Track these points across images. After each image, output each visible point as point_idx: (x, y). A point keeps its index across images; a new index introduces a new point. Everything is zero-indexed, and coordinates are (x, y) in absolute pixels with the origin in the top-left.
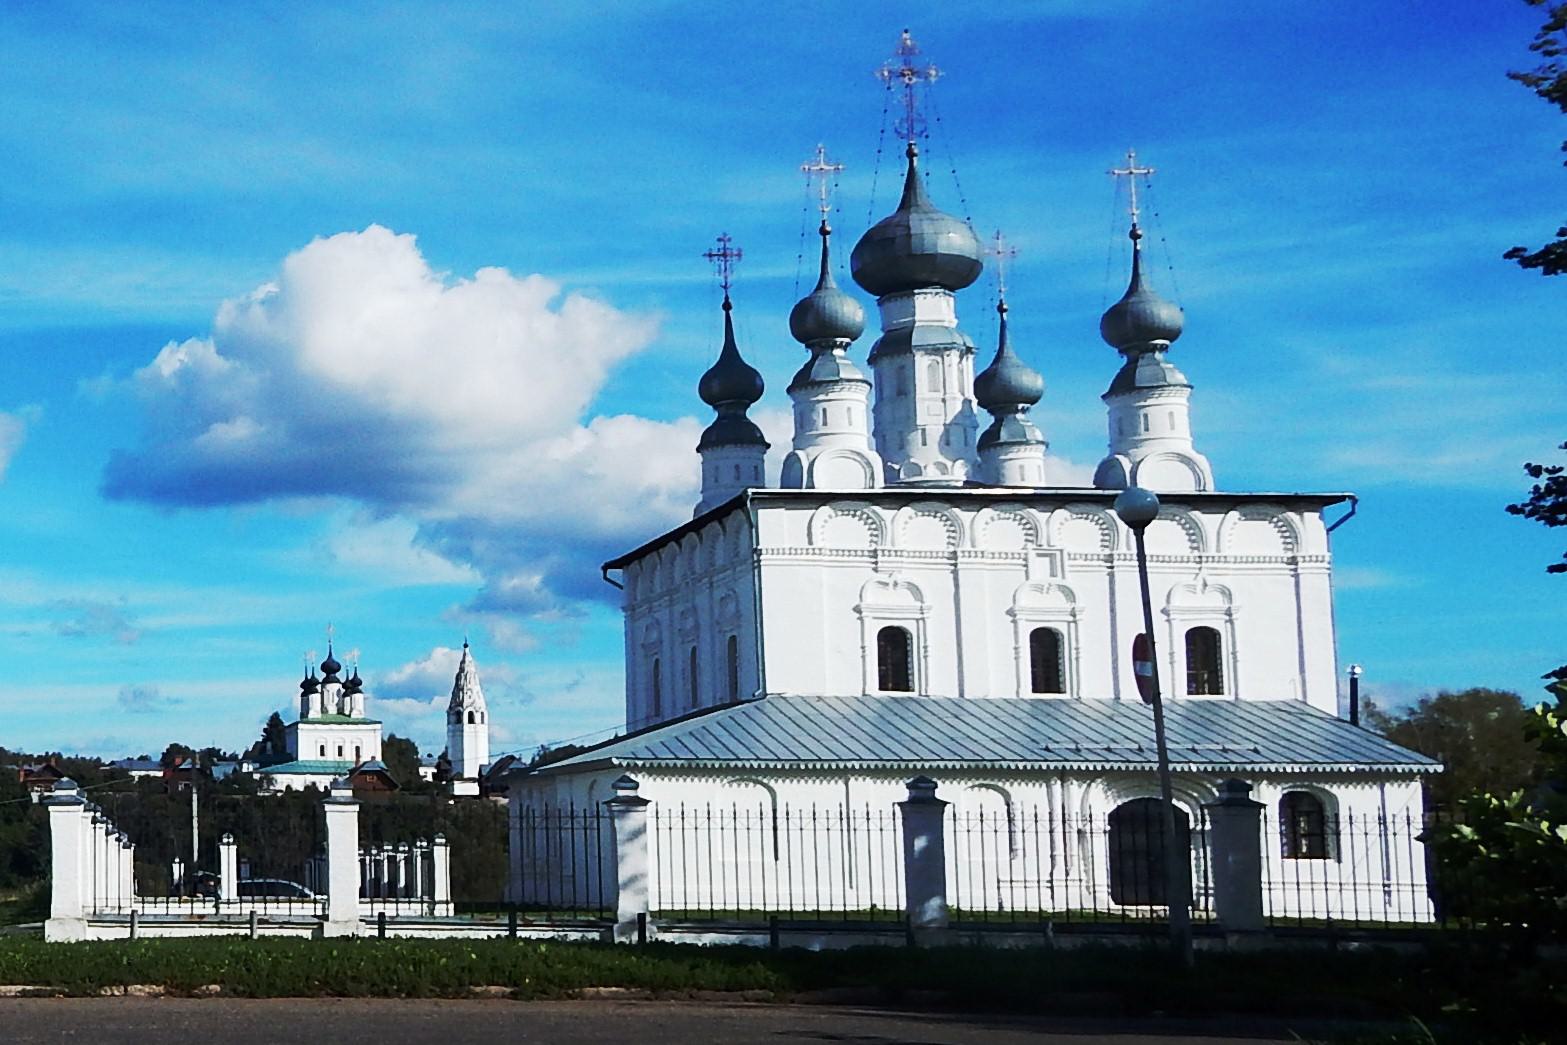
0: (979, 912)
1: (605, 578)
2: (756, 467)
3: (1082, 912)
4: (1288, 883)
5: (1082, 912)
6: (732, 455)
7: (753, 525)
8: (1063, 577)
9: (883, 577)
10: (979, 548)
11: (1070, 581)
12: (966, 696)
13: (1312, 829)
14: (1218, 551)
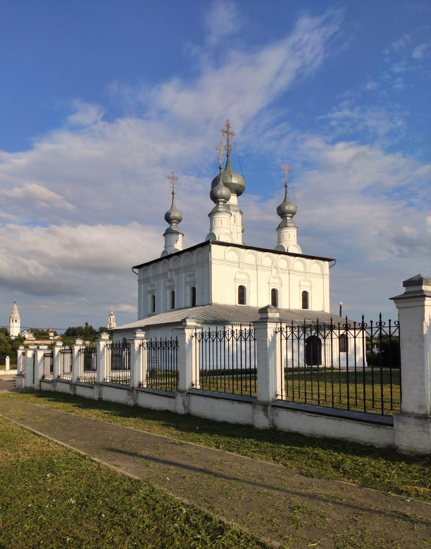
7: (210, 250)
9: (241, 271)
10: (262, 264)
11: (281, 276)
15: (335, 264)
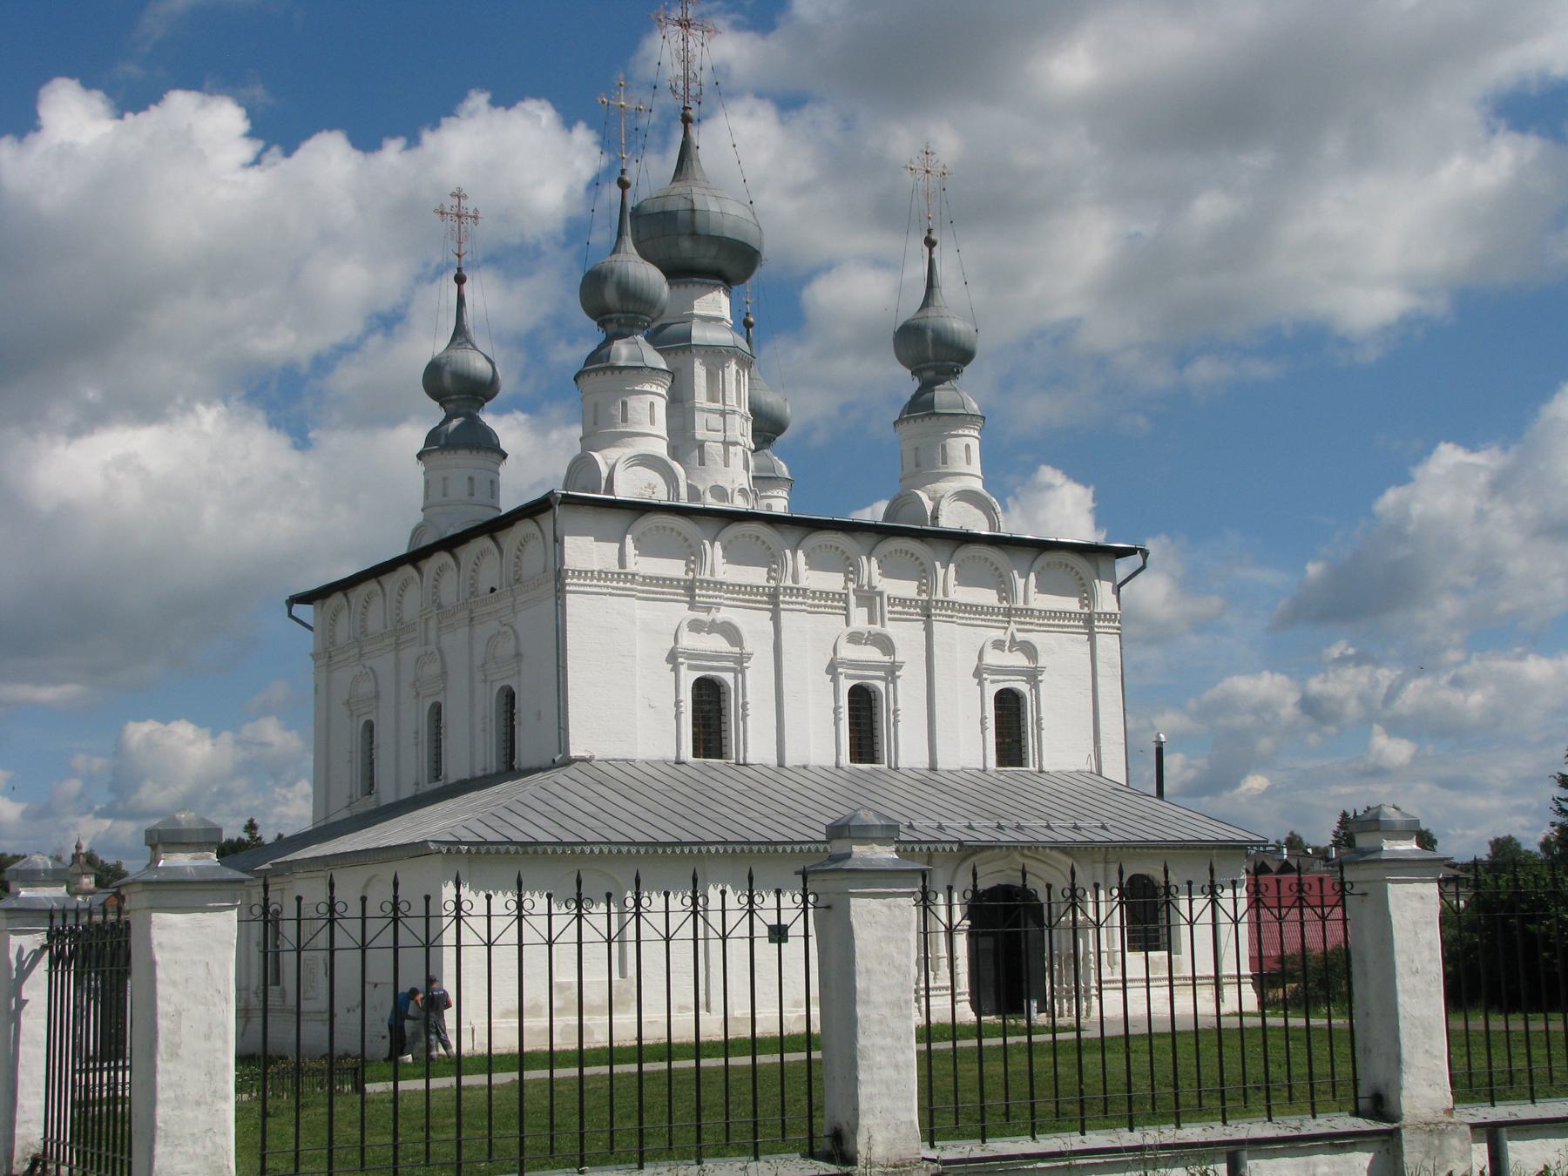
0: (565, 1052)
1: (290, 615)
2: (492, 482)
3: (1286, 1010)
4: (1132, 980)
5: (1286, 1010)
6: (462, 464)
8: (883, 625)
9: (702, 616)
11: (892, 629)
12: (787, 764)
13: (1148, 923)
14: (1026, 602)
15: (1143, 567)
